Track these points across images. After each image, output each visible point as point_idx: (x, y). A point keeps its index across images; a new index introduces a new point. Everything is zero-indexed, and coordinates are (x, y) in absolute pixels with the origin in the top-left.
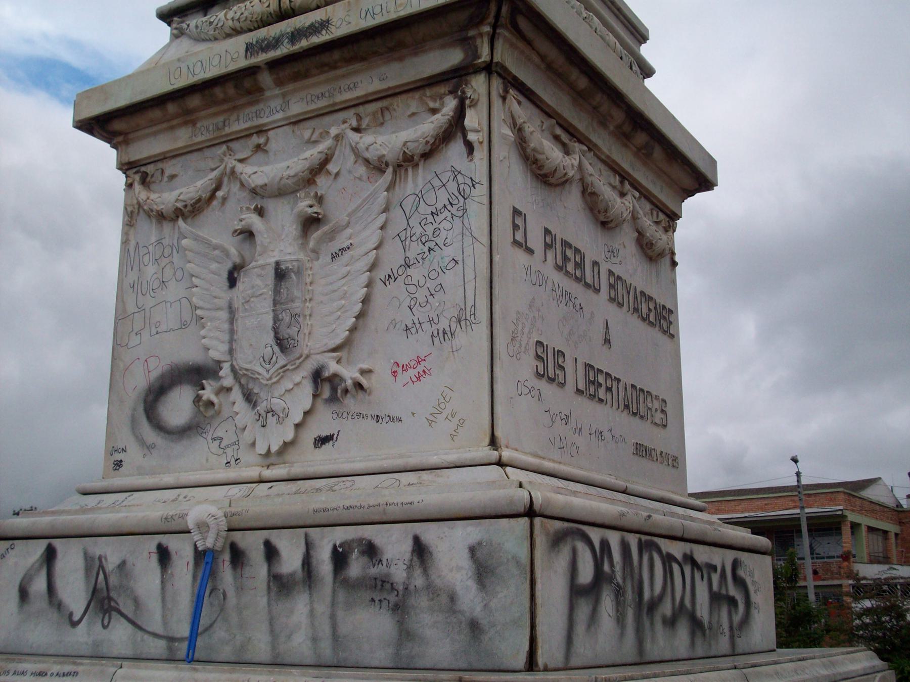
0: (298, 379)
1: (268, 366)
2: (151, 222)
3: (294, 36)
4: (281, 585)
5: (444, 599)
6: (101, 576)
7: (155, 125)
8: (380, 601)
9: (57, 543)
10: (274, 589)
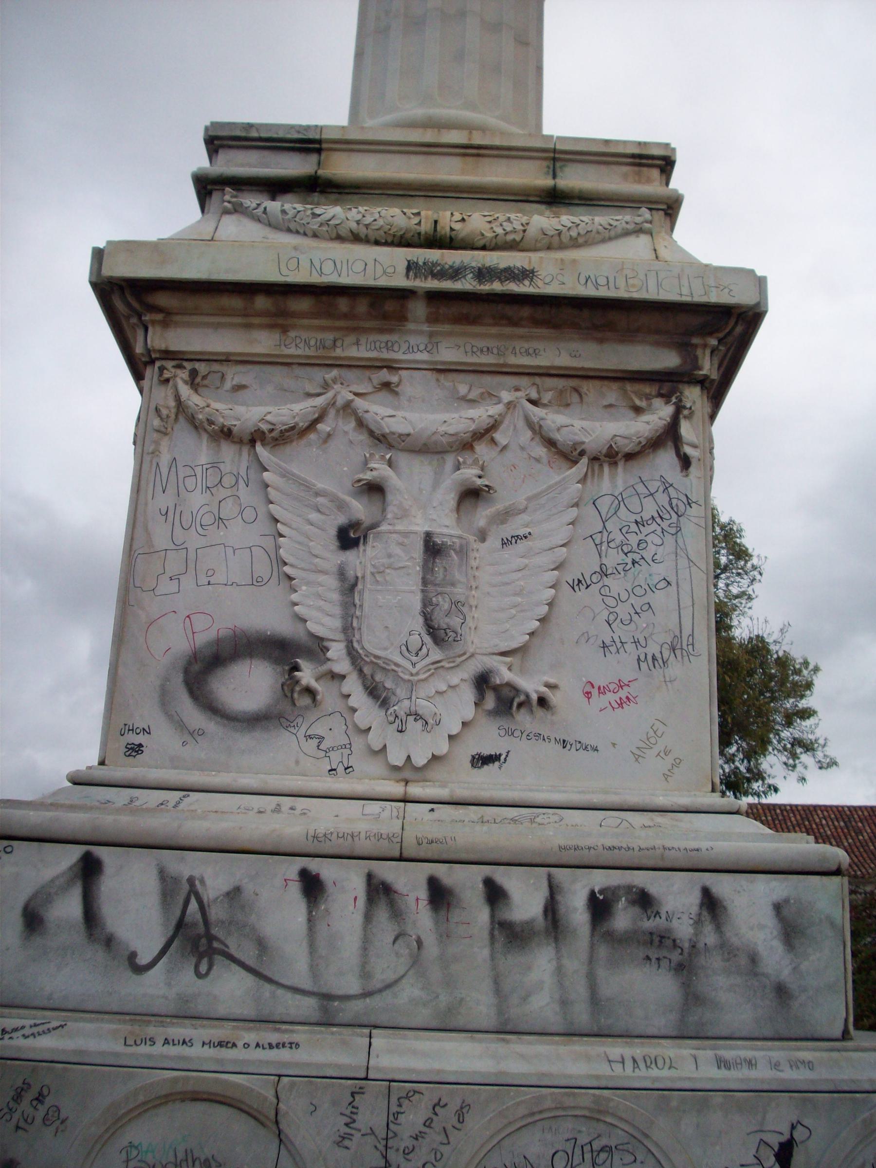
0: (455, 681)
1: (414, 659)
2: (200, 437)
3: (482, 274)
4: (511, 935)
5: (743, 961)
6: (193, 905)
7: (224, 315)
8: (658, 959)
9: (101, 852)
10: (501, 938)
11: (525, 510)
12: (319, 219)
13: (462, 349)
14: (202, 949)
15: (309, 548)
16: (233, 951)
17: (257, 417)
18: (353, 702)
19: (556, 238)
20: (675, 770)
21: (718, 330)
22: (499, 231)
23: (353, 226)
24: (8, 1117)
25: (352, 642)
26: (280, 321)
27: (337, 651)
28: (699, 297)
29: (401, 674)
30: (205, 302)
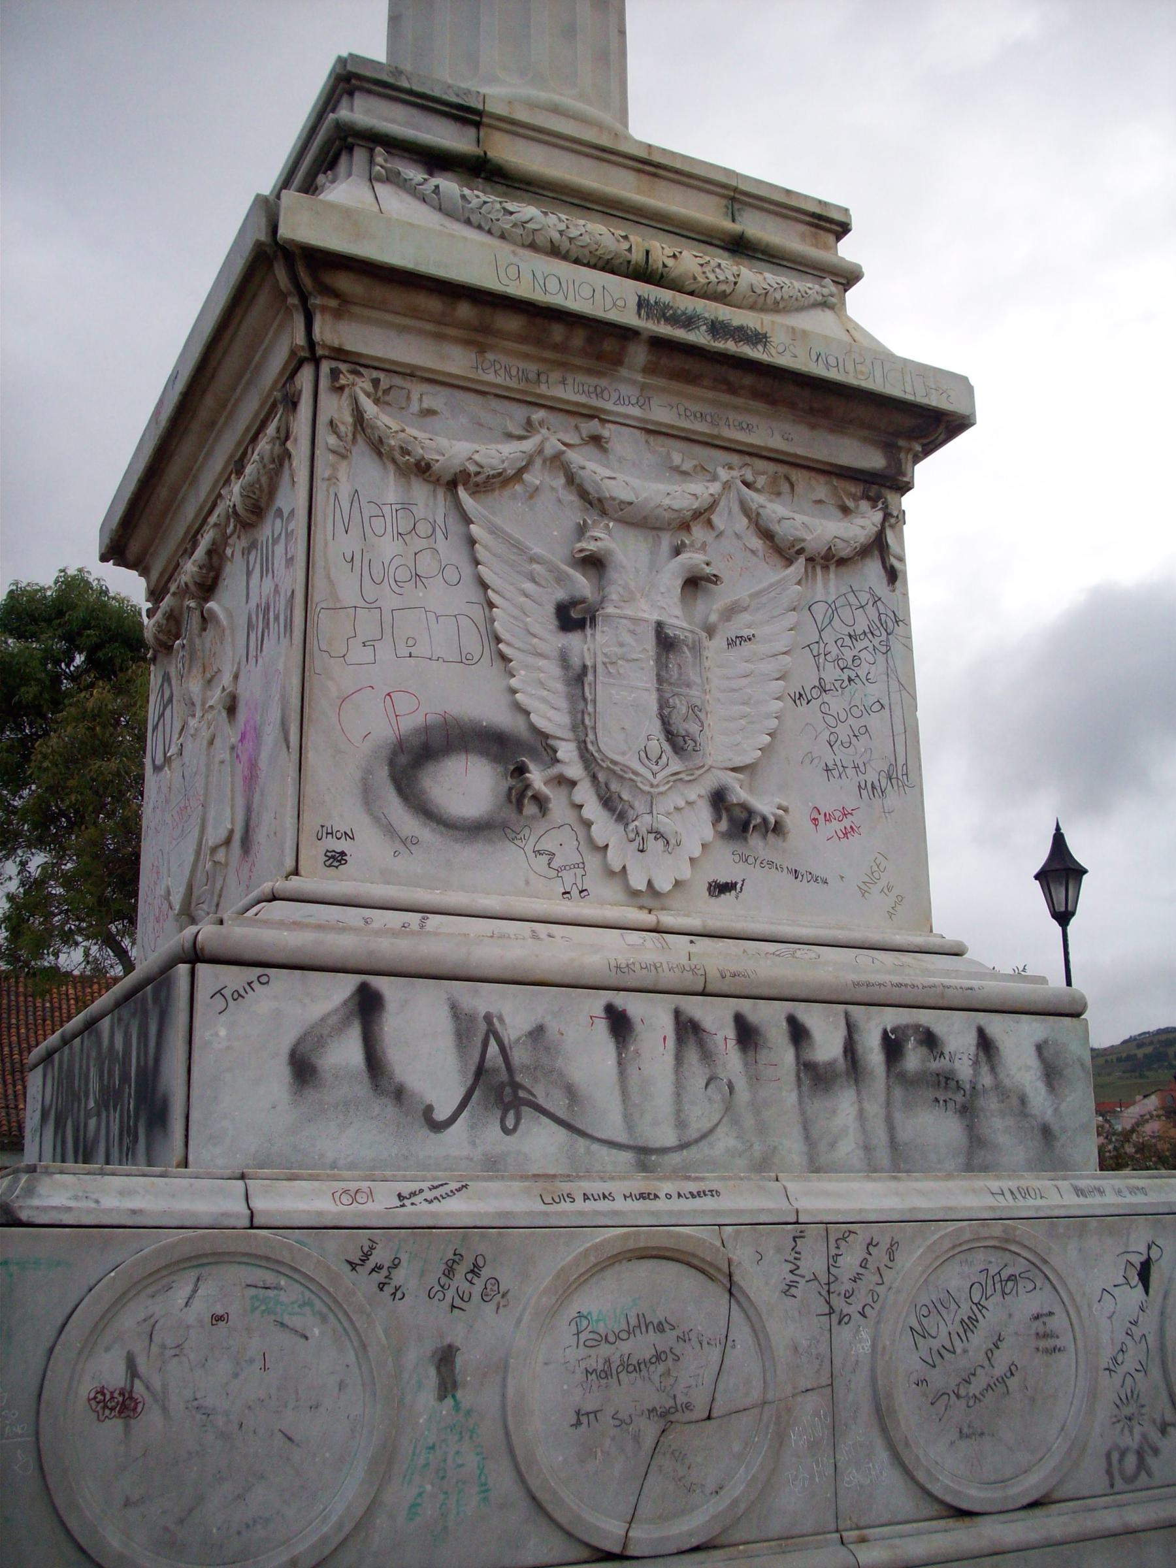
0: (693, 797)
1: (655, 768)
3: (717, 328)
4: (815, 1077)
5: (1014, 1101)
6: (493, 1048)
7: (417, 318)
10: (807, 1082)
11: (746, 609)
12: (512, 217)
13: (675, 409)
14: (507, 1100)
15: (526, 624)
16: (541, 1101)
17: (466, 455)
18: (587, 813)
19: (762, 297)
20: (898, 908)
21: (925, 437)
22: (712, 277)
23: (556, 236)
24: (440, 1295)
25: (585, 742)
26: (480, 339)
27: (567, 751)
28: (921, 399)
29: (639, 784)
30: (397, 297)
